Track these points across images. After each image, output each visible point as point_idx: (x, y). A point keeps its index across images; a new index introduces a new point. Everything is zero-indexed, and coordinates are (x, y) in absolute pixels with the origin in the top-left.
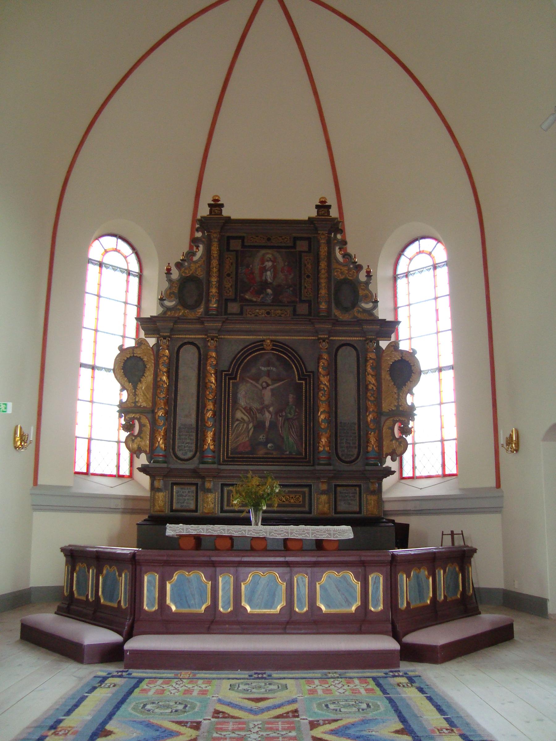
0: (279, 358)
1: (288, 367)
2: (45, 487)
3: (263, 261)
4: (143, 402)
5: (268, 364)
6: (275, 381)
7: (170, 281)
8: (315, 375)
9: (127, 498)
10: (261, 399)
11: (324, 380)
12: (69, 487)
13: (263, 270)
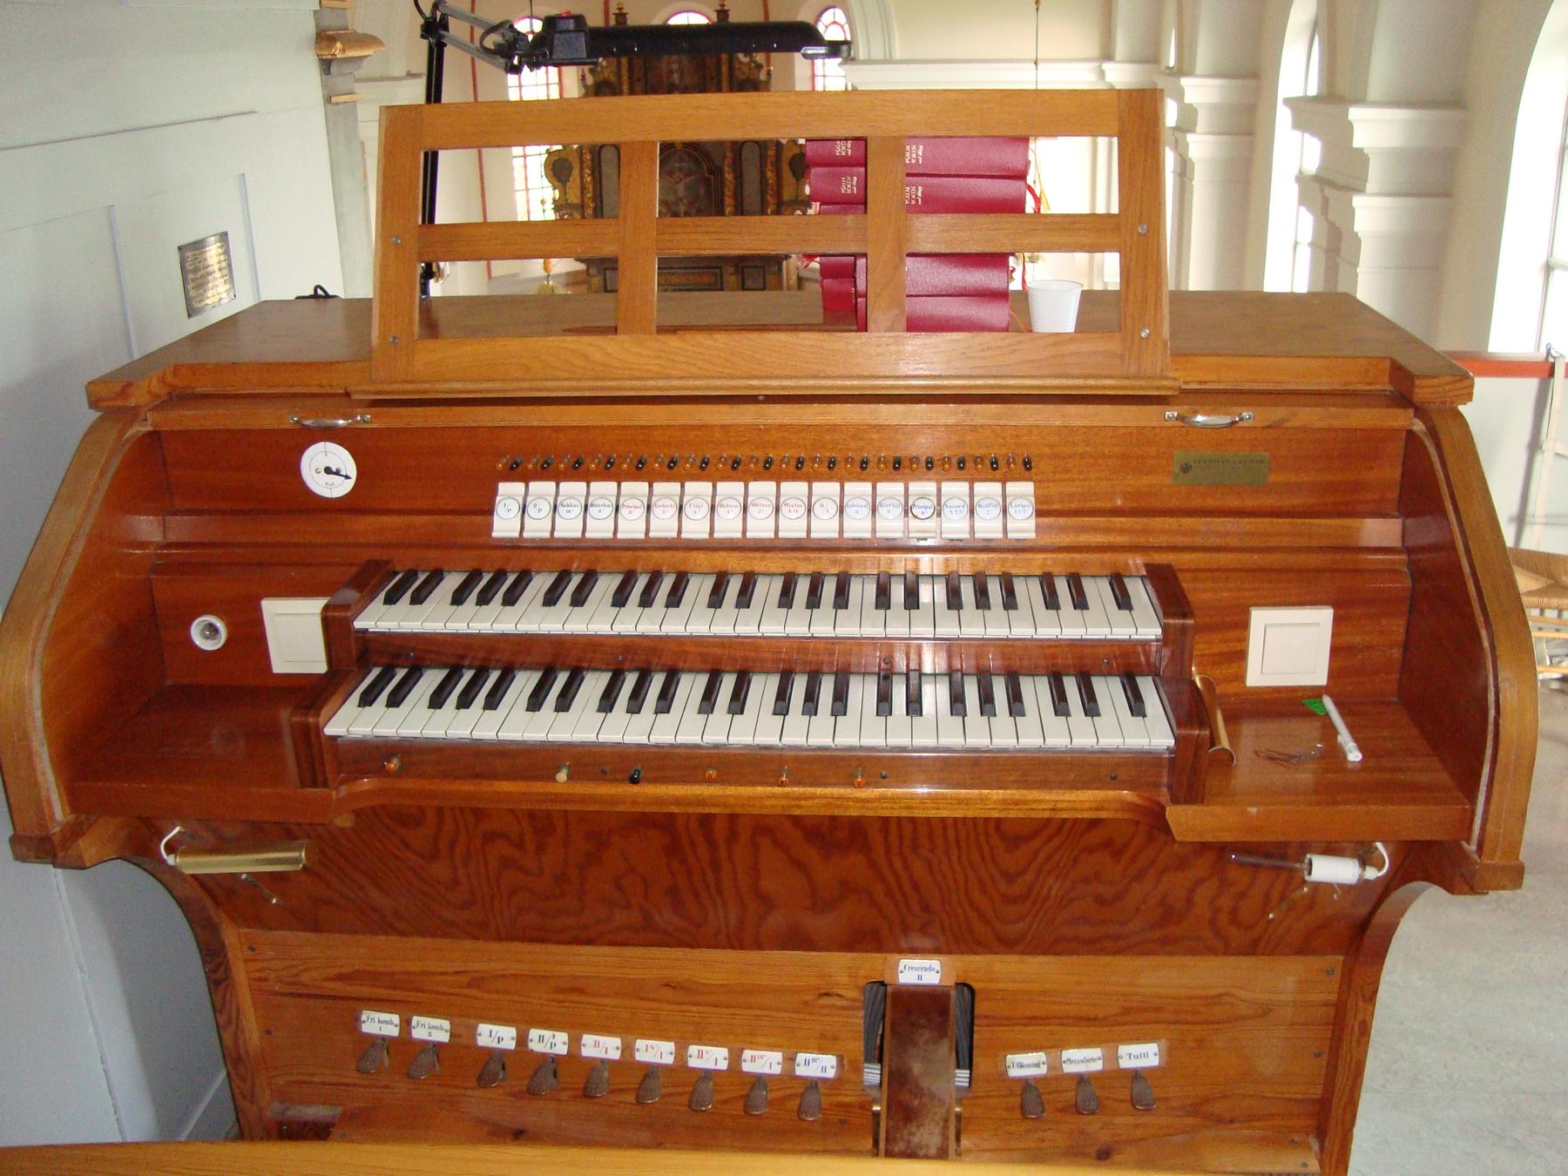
0: (689, 154)
1: (696, 161)
2: (498, 278)
3: (669, 64)
4: (574, 198)
5: (681, 160)
6: (686, 175)
7: (585, 86)
8: (722, 169)
9: (568, 274)
10: (675, 192)
11: (729, 177)
12: (516, 275)
13: (671, 72)
